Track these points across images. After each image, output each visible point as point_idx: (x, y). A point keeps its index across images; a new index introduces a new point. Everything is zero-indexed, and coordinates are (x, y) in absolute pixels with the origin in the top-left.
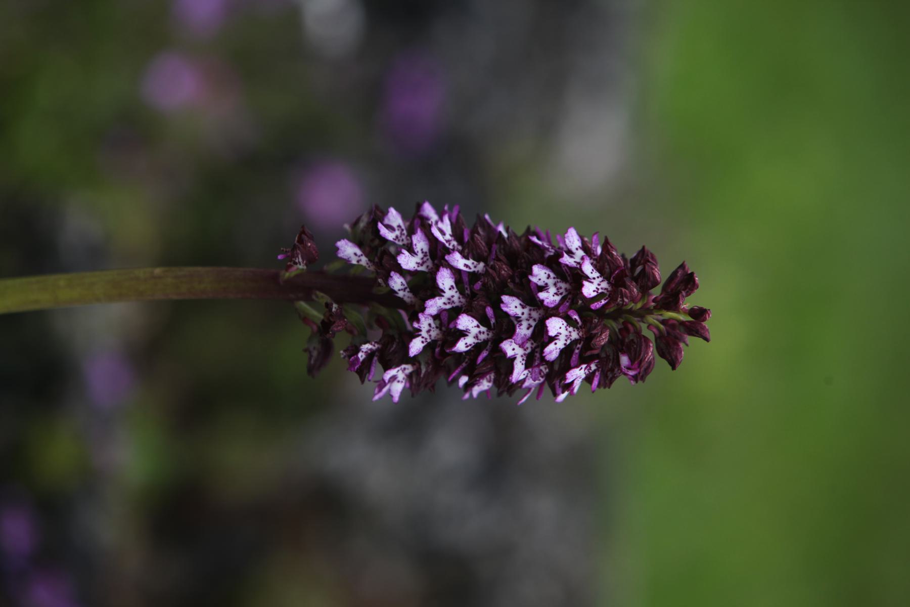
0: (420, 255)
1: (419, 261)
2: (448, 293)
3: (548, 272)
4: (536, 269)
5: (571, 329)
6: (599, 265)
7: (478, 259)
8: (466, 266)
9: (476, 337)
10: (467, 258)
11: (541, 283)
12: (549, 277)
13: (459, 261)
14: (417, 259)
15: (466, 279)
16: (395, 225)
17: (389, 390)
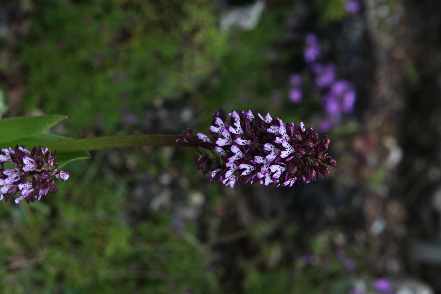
0: (227, 138)
2: (237, 154)
3: (271, 145)
4: (266, 145)
5: (282, 167)
6: (290, 142)
7: (248, 139)
8: (243, 143)
9: (250, 170)
10: (243, 139)
11: (269, 150)
12: (272, 148)
13: (240, 141)
14: (226, 140)
15: (244, 147)
16: (219, 125)
17: (256, 176)
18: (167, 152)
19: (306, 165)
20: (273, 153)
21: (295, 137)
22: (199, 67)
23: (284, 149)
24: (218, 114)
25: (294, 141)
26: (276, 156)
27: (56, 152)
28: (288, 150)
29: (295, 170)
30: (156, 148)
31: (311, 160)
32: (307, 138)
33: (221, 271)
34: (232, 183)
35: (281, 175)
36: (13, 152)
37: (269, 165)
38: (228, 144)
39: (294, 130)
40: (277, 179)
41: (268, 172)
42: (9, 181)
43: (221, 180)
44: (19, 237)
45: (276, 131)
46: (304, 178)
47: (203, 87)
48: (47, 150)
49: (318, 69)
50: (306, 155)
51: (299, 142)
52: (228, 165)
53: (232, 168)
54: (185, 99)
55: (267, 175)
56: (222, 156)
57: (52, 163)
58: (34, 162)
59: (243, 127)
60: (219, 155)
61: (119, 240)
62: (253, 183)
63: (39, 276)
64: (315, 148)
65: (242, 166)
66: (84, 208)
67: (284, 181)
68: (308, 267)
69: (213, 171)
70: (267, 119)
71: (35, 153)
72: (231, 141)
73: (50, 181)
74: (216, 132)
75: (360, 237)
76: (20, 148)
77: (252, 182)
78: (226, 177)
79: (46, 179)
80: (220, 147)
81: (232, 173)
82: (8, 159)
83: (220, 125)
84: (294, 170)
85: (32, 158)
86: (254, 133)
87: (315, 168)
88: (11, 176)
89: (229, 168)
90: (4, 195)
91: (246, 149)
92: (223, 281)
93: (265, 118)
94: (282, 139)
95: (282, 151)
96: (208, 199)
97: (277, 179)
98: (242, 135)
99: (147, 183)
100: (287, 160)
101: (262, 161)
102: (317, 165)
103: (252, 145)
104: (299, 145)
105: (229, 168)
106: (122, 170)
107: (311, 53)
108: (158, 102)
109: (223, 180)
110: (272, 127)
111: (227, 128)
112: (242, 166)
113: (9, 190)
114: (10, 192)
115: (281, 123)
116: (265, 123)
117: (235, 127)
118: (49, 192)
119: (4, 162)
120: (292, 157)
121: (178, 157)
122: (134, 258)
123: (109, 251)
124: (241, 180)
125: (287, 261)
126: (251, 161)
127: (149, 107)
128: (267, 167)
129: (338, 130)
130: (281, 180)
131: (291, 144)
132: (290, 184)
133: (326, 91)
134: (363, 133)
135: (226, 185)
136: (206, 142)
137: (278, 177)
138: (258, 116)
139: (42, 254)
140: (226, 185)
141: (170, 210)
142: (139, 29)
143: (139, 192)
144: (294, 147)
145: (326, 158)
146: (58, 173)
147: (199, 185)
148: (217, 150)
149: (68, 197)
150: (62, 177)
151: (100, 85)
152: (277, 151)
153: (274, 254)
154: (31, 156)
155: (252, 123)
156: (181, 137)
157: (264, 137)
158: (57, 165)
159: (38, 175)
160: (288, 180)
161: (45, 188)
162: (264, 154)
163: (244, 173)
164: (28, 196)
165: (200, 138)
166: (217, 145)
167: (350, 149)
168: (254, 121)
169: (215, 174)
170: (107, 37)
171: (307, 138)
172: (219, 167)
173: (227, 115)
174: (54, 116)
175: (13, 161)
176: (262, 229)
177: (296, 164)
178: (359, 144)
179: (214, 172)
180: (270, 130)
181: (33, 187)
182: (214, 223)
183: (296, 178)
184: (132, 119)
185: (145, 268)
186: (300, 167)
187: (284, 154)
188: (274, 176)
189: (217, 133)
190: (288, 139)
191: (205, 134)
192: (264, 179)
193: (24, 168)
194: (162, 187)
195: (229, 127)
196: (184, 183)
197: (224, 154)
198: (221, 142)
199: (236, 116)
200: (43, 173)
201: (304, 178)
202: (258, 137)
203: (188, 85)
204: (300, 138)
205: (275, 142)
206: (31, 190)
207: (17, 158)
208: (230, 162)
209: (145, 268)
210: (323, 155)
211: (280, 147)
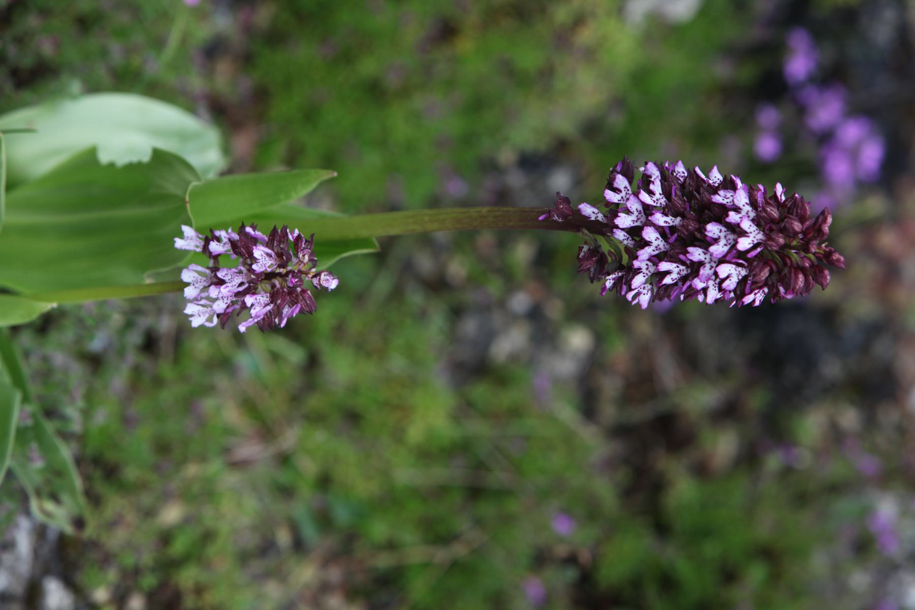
0: (636, 213)
1: (635, 219)
2: (655, 243)
3: (720, 227)
5: (740, 269)
6: (756, 221)
8: (666, 222)
9: (678, 273)
10: (666, 215)
11: (715, 236)
12: (721, 231)
13: (660, 219)
14: (634, 217)
15: (668, 231)
17: (690, 286)
18: (522, 252)
19: (785, 264)
20: (723, 241)
21: (766, 211)
22: (585, 92)
23: (744, 234)
24: (618, 169)
25: (763, 218)
26: (729, 246)
27: (315, 237)
28: (752, 236)
29: (765, 274)
30: (504, 241)
31: (795, 255)
32: (788, 213)
33: (622, 475)
34: (645, 299)
35: (738, 283)
36: (236, 237)
37: (714, 265)
38: (638, 224)
39: (765, 198)
40: (730, 292)
41: (713, 277)
42: (228, 289)
43: (623, 293)
44: (249, 405)
45: (729, 200)
46: (782, 289)
47: (592, 129)
48: (297, 232)
49: (811, 95)
50: (787, 246)
51: (772, 220)
52: (636, 264)
53: (644, 270)
54: (558, 152)
55: (711, 283)
56: (627, 249)
57: (307, 257)
58: (273, 254)
59: (666, 193)
60: (620, 245)
61: (433, 414)
62: (685, 298)
63: (284, 477)
64: (803, 232)
65: (664, 266)
66: (369, 355)
67: (744, 295)
68: (787, 472)
69: (609, 275)
70: (712, 178)
71: (276, 238)
72: (643, 219)
73: (304, 291)
74: (616, 201)
75: (889, 416)
76: (249, 230)
77: (682, 297)
78: (633, 287)
79: (295, 287)
80: (623, 229)
81: (644, 279)
82: (225, 249)
83: (623, 189)
84: (762, 274)
85: (269, 248)
86: (687, 204)
87: (803, 270)
88: (231, 280)
89: (638, 271)
90: (218, 316)
91: (672, 234)
92: (627, 493)
93: (708, 176)
94: (740, 215)
95: (740, 237)
96: (599, 339)
97: (730, 292)
98: (664, 208)
99: (485, 309)
100: (750, 255)
101: (702, 257)
102: (807, 265)
103: (683, 226)
104: (774, 227)
105: (638, 271)
106: (438, 285)
107: (799, 64)
108: (506, 156)
109: (626, 293)
110: (722, 193)
111: (636, 194)
112: (664, 266)
113: (228, 307)
114: (230, 310)
115: (739, 184)
116: (709, 185)
117: (651, 193)
118: (301, 311)
119: (219, 255)
120: (759, 250)
121: (544, 260)
122: (461, 449)
123: (415, 433)
124: (660, 291)
125: (749, 458)
126: (682, 257)
127: (489, 166)
128: (712, 267)
129: (851, 211)
130: (738, 292)
131: (757, 225)
132: (754, 301)
133: (826, 138)
134: (896, 220)
135: (634, 303)
136: (597, 221)
137: (732, 287)
138: (695, 171)
139: (290, 438)
140: (634, 303)
141: (527, 360)
142: (472, 18)
143: (470, 326)
144: (763, 231)
145: (825, 251)
146: (317, 275)
147: (583, 312)
148: (616, 236)
149: (339, 332)
150: (325, 284)
151: (399, 123)
152: (731, 237)
153: (723, 445)
154: (269, 245)
155: (683, 186)
156: (549, 212)
157: (706, 211)
158: (316, 261)
159: (280, 279)
160: (750, 293)
161: (293, 303)
162: (706, 243)
163: (668, 280)
164: (263, 319)
165: (584, 213)
166: (617, 227)
167: (870, 250)
168: (688, 181)
169: (612, 282)
170: (414, 32)
171: (788, 213)
172: (621, 267)
173: (635, 170)
174: (312, 171)
175: (235, 253)
176: (700, 399)
177: (766, 263)
178: (888, 240)
179: (610, 277)
180: (718, 199)
181: (272, 303)
182: (610, 387)
183: (766, 290)
184: (457, 188)
185: (480, 466)
186: (774, 267)
187: (744, 244)
188: (725, 285)
189: (617, 205)
190: (752, 214)
191: (593, 206)
192: (705, 290)
193: (254, 267)
194: (514, 318)
195: (639, 193)
196: (555, 310)
197: (630, 243)
198: (624, 221)
199: (655, 172)
200: (290, 276)
201: (782, 289)
202: (695, 210)
203: (564, 123)
204: (774, 213)
205: (728, 220)
206: (269, 308)
207: (242, 248)
208: (640, 258)
209: (480, 466)
210: (819, 245)
211: (737, 229)
